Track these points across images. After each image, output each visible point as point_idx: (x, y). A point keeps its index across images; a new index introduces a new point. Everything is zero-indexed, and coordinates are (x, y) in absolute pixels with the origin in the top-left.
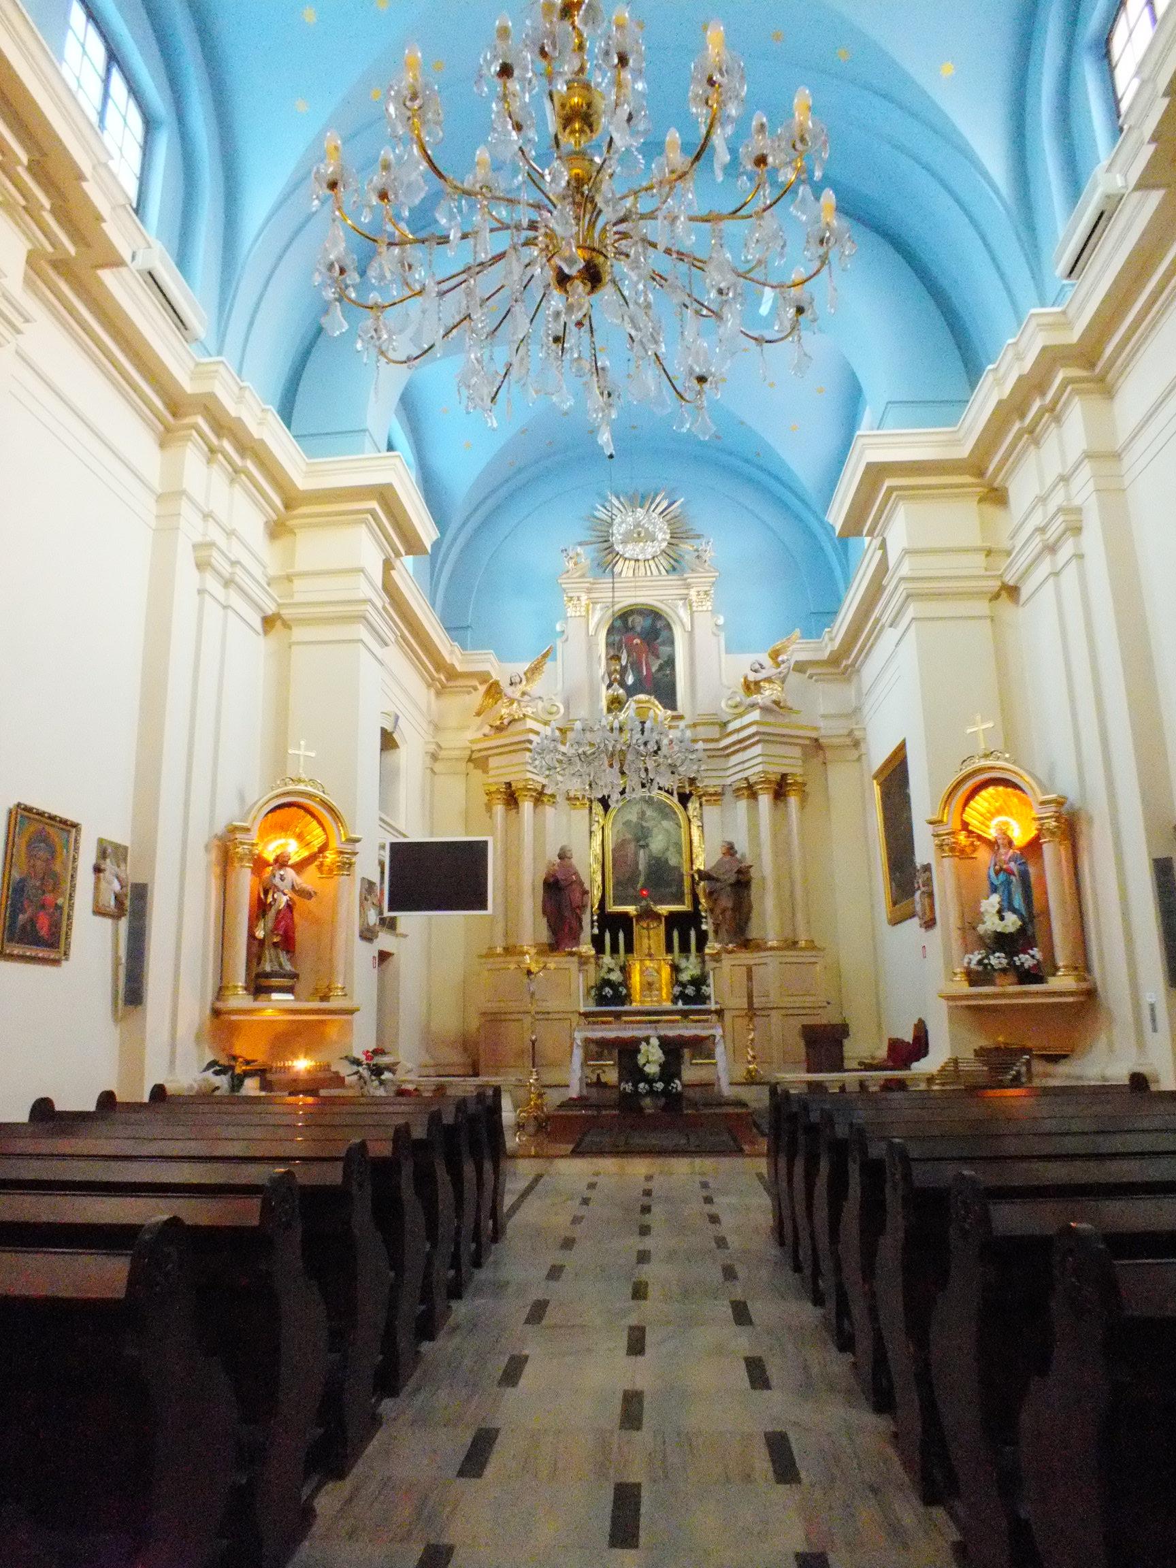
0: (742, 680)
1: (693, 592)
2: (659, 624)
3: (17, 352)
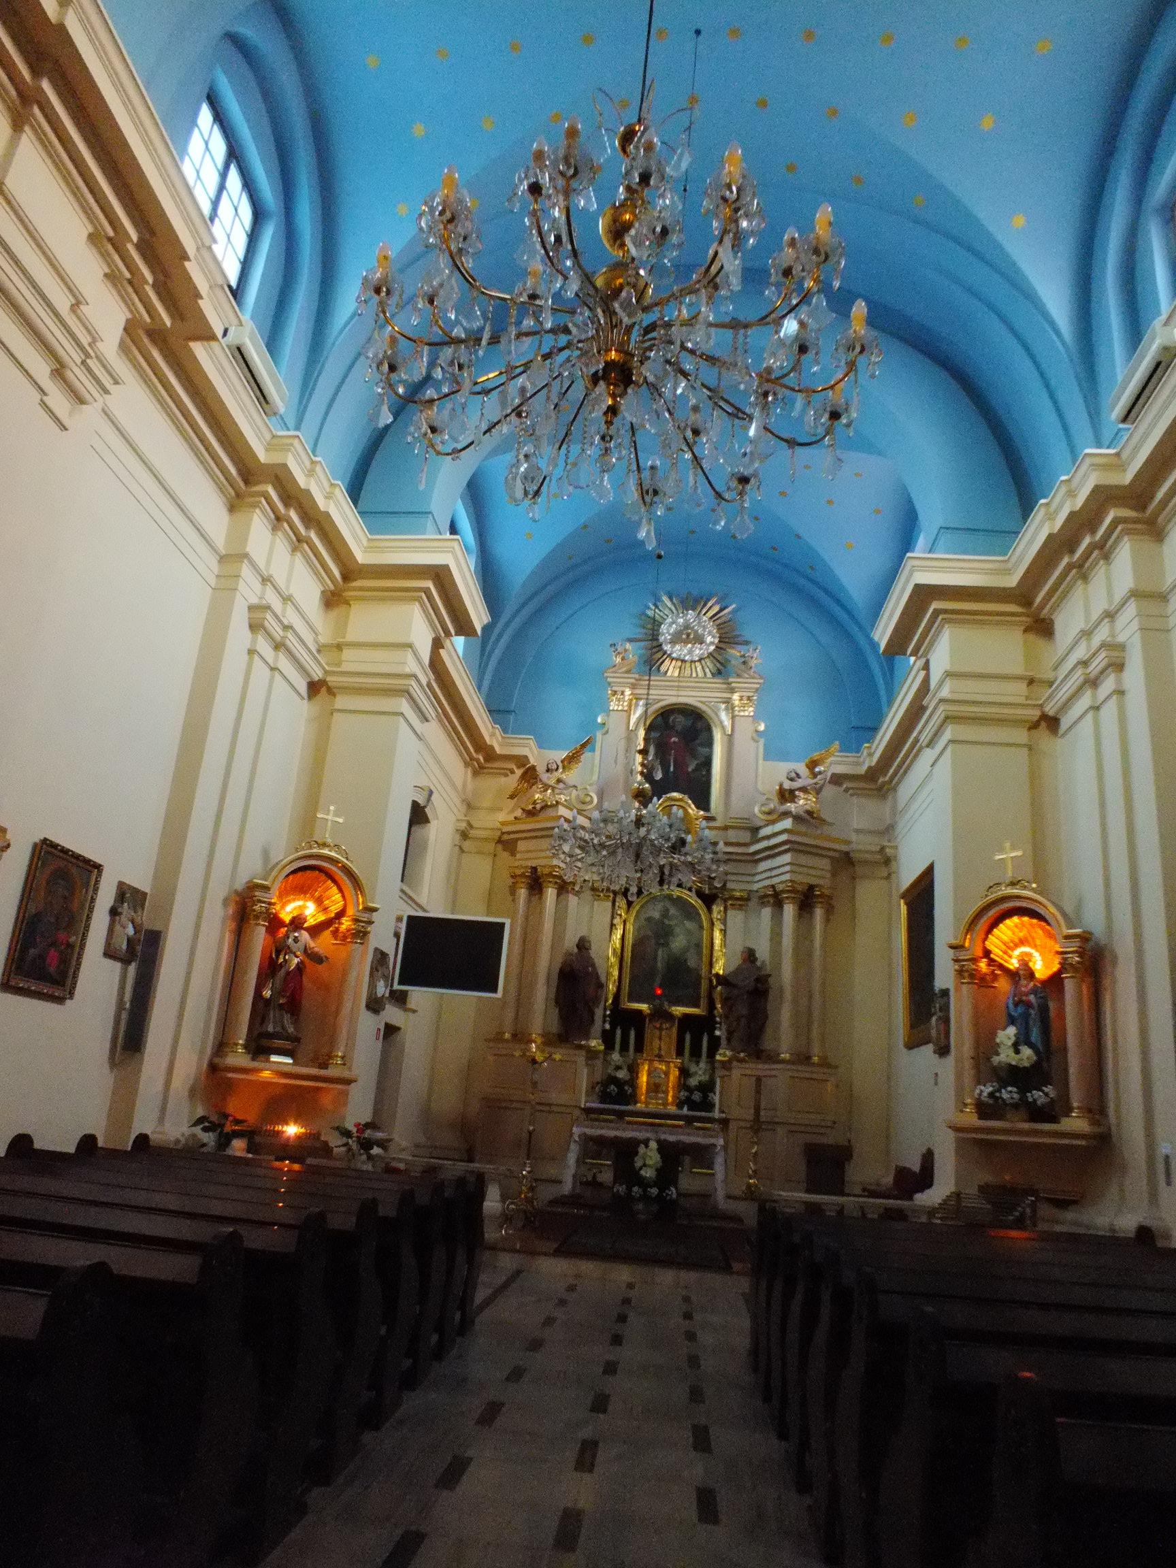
0: (778, 787)
2: (699, 725)
3: (103, 410)
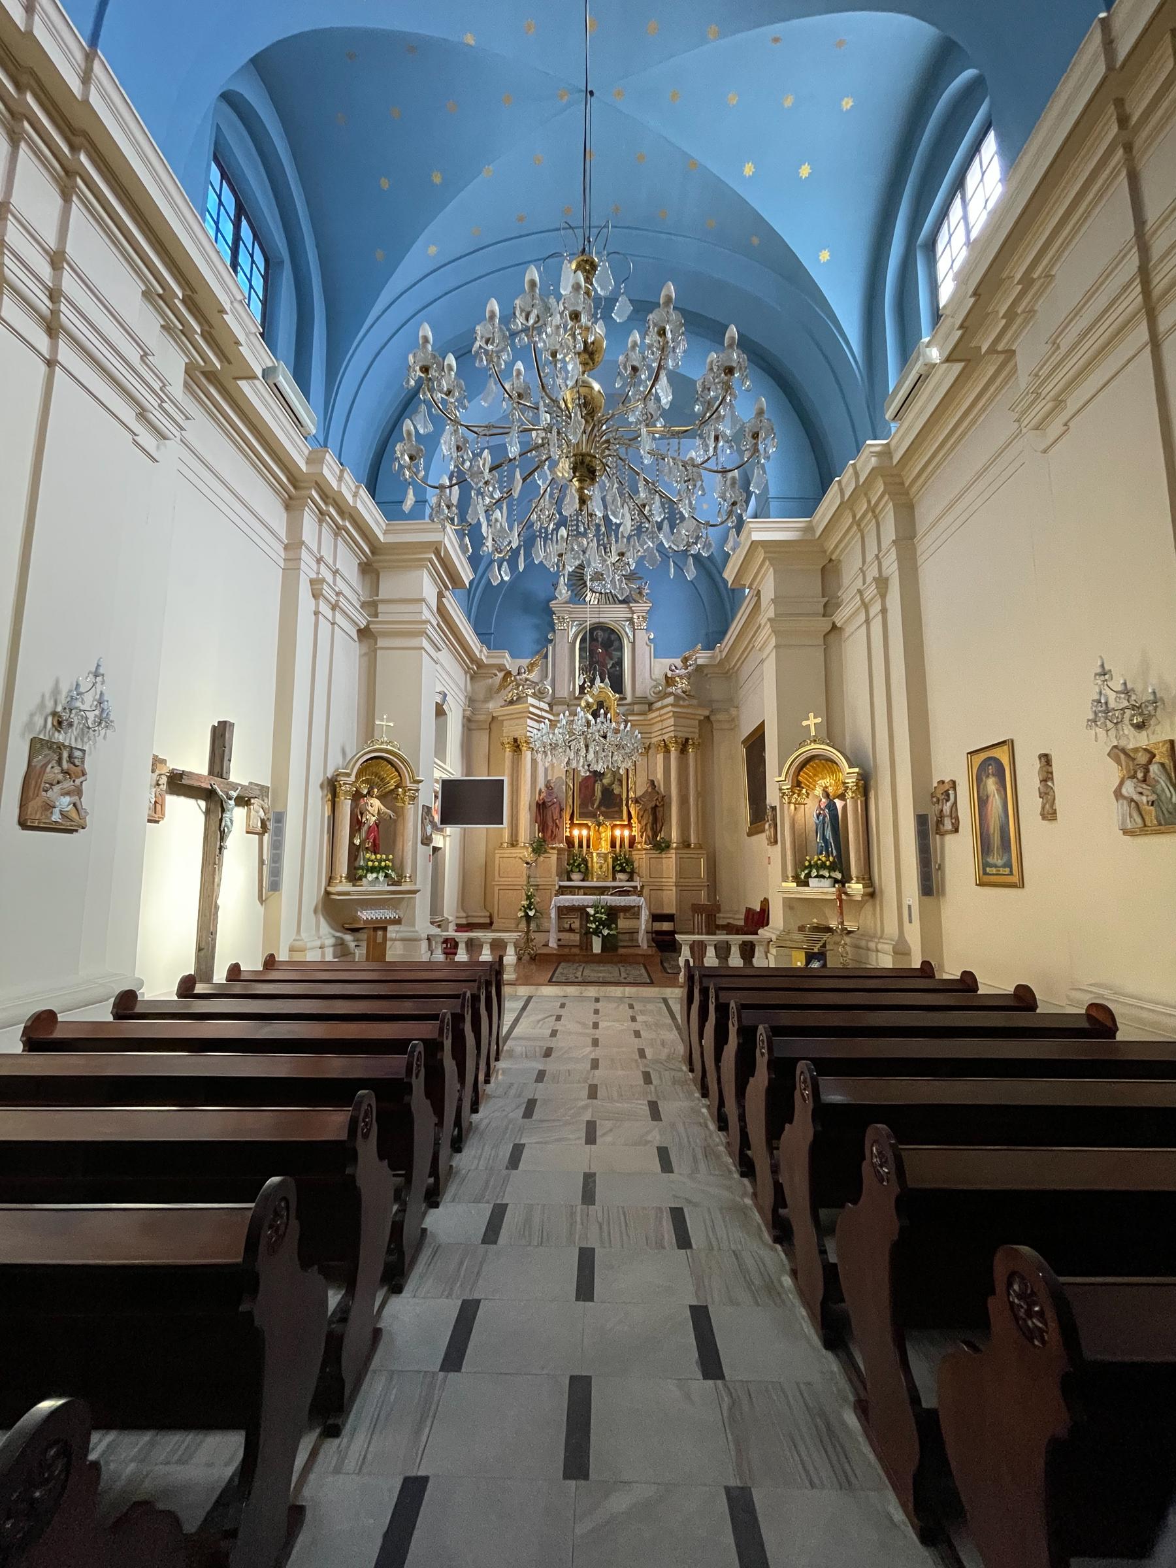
1: (635, 616)
2: (613, 637)
3: (181, 440)
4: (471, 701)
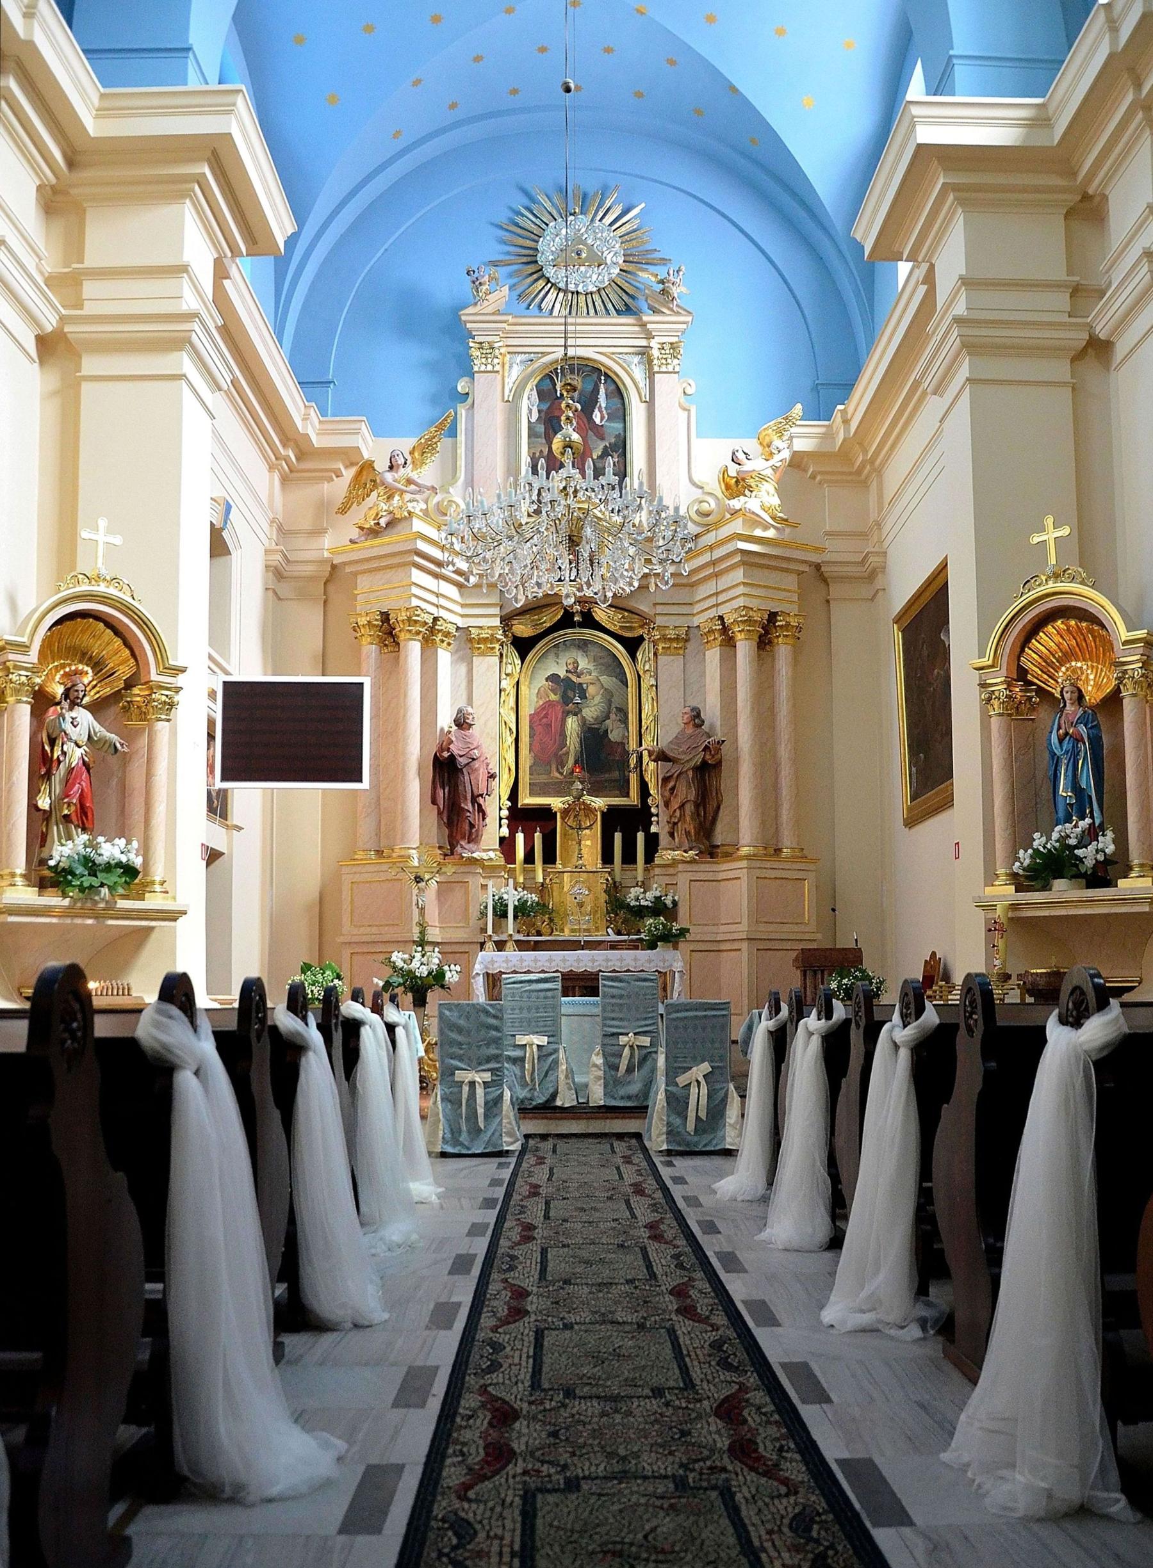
1: (654, 343)
4: (283, 531)
